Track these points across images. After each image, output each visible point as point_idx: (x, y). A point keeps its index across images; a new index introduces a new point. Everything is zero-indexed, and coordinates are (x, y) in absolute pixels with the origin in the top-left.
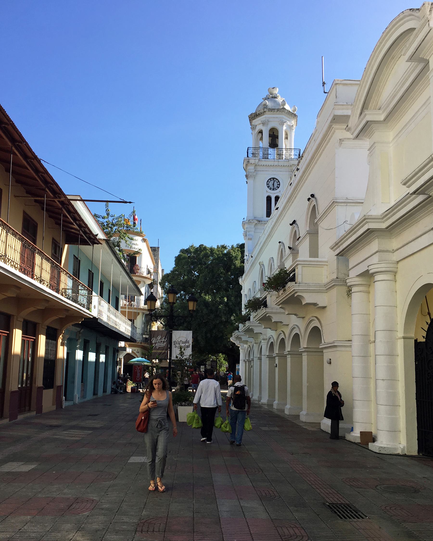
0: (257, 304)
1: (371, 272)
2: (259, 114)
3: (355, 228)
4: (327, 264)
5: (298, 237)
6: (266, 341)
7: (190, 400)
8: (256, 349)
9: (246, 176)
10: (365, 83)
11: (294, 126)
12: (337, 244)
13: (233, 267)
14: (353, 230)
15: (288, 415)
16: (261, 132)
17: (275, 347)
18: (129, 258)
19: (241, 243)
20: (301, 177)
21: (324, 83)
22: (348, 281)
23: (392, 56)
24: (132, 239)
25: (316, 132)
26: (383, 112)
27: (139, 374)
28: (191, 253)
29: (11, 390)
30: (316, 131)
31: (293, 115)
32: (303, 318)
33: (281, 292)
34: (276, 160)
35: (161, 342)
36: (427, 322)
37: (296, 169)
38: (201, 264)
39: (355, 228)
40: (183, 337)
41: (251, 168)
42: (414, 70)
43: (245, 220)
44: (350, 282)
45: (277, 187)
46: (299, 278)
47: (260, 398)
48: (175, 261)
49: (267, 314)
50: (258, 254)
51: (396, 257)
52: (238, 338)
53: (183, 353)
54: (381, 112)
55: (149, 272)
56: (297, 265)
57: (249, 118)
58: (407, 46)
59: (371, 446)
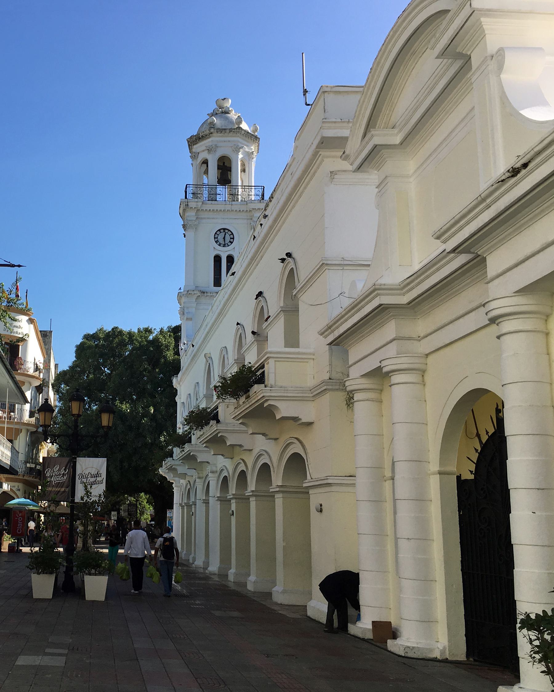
0: (202, 418)
1: (385, 370)
2: (202, 136)
3: (359, 303)
4: (312, 357)
5: (266, 317)
6: (217, 475)
7: (103, 565)
8: (200, 485)
9: (184, 226)
10: (370, 91)
11: (255, 154)
12: (330, 328)
13: (163, 360)
14: (355, 307)
15: (254, 592)
16: (205, 162)
17: (230, 485)
18: (8, 347)
19: (174, 325)
20: (271, 227)
21: (305, 92)
22: (347, 384)
23: (411, 51)
24: (15, 320)
25: (292, 162)
26: (400, 131)
27: (20, 524)
28: (99, 339)
30: (294, 160)
31: (253, 138)
32: (276, 439)
33: (242, 399)
34: (228, 203)
35: (60, 475)
36: (475, 449)
37: (262, 216)
38: (114, 356)
39: (359, 303)
40: (93, 468)
41: (191, 214)
42: (447, 70)
43: (182, 291)
44: (351, 385)
45: (230, 242)
46: (270, 379)
47: (207, 564)
48: (77, 352)
49: (219, 432)
50: (203, 342)
51: (424, 347)
52: (171, 469)
53: (91, 493)
54: (396, 131)
55: (37, 369)
56: (268, 358)
57: (188, 142)
58: (438, 35)
59: (391, 644)
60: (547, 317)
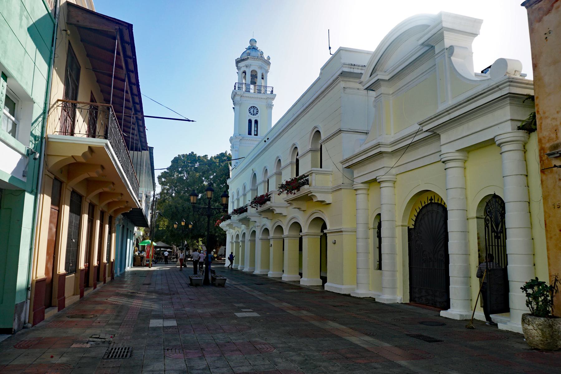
16: (245, 72)
21: (330, 48)
29: (36, 277)
60: (465, 161)
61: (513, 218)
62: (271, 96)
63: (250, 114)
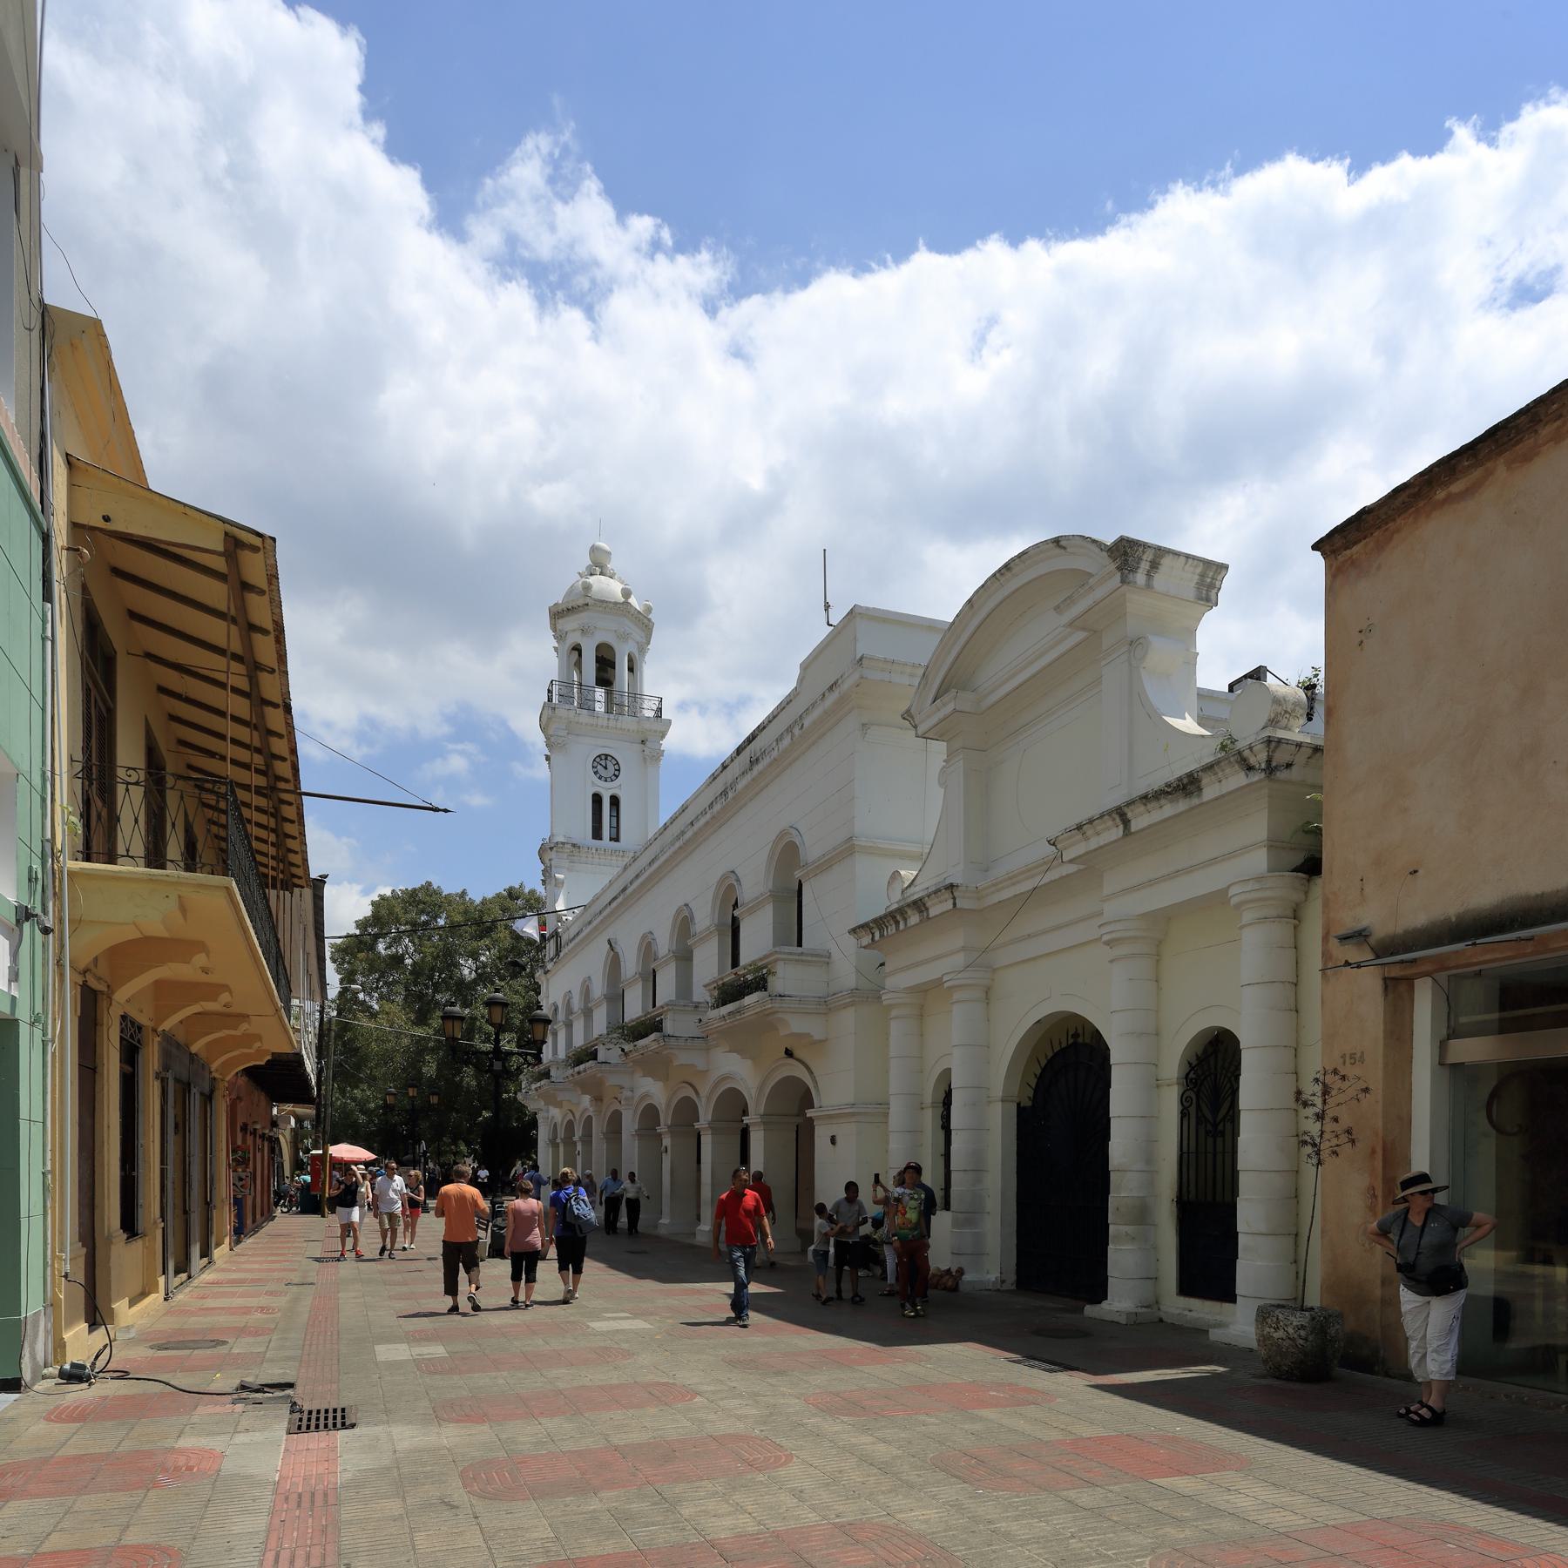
21: (827, 607)
61: (1256, 1089)
62: (657, 726)
63: (595, 779)
